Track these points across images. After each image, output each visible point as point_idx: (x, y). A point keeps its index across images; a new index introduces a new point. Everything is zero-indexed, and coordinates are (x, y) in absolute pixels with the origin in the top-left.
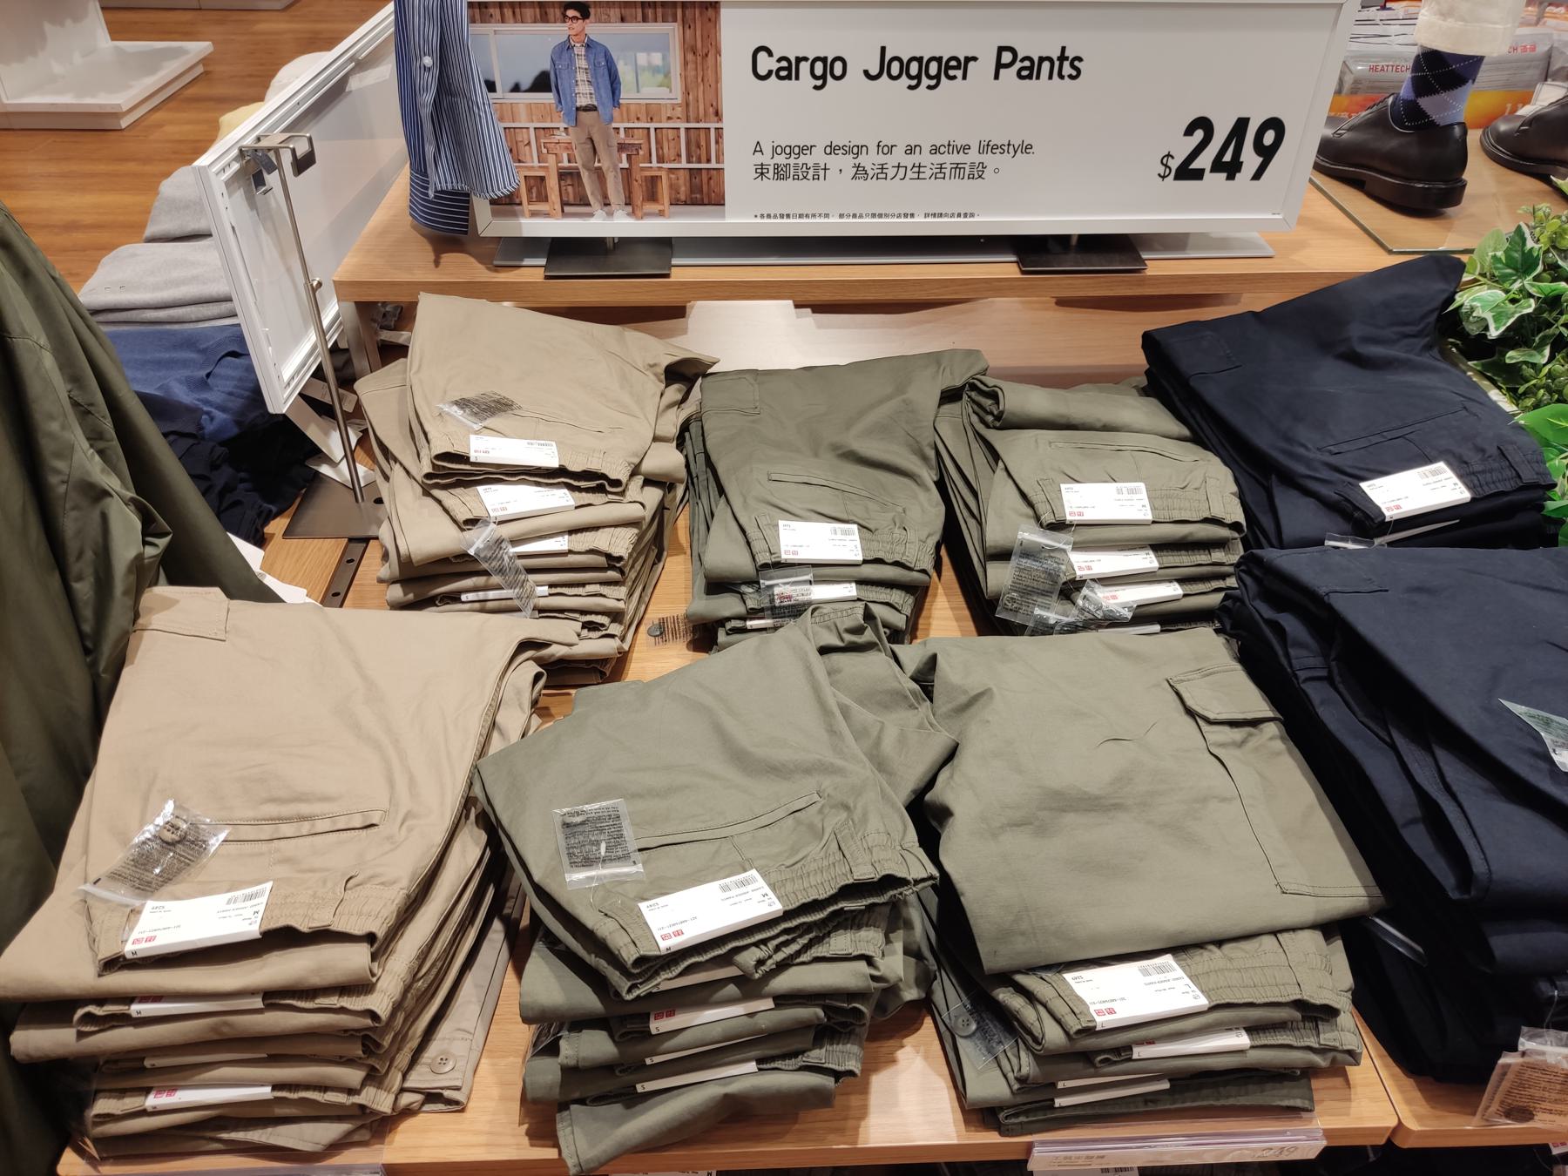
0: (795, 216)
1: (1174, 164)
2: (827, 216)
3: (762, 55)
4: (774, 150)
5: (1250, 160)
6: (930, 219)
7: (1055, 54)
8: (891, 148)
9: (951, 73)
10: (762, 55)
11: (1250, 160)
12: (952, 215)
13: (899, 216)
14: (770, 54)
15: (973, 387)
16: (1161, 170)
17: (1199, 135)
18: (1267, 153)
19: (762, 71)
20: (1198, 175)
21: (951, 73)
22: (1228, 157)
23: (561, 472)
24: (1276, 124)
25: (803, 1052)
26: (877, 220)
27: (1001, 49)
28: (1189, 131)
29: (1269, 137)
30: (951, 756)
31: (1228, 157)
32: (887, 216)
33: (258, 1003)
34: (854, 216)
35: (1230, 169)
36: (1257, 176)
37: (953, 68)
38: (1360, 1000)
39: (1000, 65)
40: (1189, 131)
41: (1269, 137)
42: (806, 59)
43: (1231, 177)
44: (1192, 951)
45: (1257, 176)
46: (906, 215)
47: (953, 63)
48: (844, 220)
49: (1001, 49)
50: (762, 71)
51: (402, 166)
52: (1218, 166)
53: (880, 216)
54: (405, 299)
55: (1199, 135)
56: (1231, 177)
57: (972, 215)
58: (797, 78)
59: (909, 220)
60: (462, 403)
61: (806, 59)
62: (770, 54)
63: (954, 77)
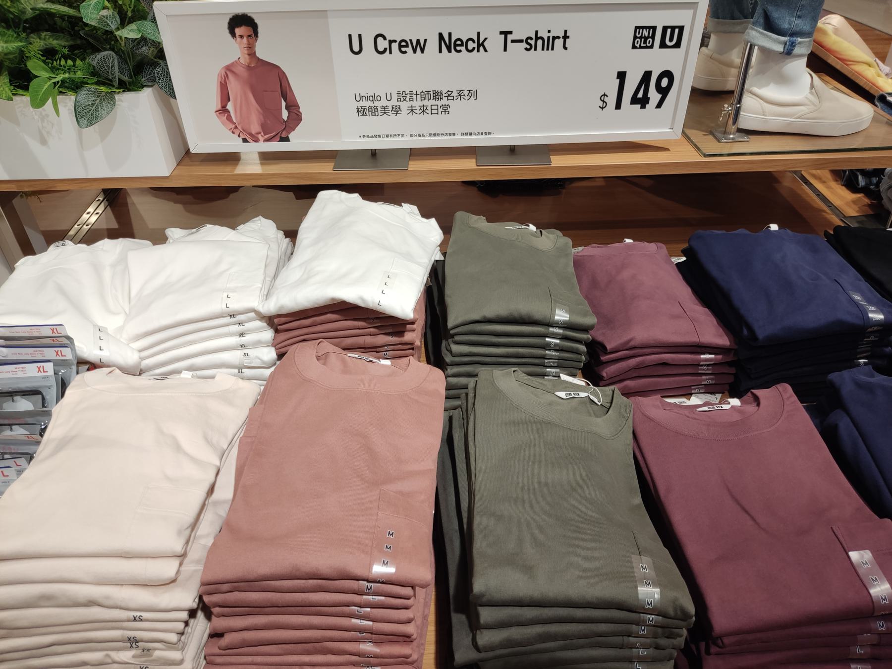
0: (383, 136)
2: (403, 135)
3: (380, 39)
5: (654, 96)
6: (465, 137)
7: (562, 34)
9: (458, 48)
10: (380, 39)
11: (654, 96)
12: (478, 134)
13: (446, 135)
14: (385, 38)
15: (223, 110)
16: (601, 103)
18: (664, 92)
19: (381, 49)
21: (458, 48)
22: (640, 95)
26: (433, 138)
29: (665, 82)
31: (640, 95)
32: (439, 135)
34: (419, 135)
35: (641, 101)
36: (659, 105)
37: (404, 46)
38: (696, 615)
41: (665, 82)
42: (395, 41)
43: (643, 107)
45: (659, 105)
46: (450, 135)
47: (459, 42)
48: (414, 138)
50: (381, 49)
51: (63, 444)
52: (634, 100)
53: (435, 135)
54: (135, 231)
56: (643, 107)
57: (490, 133)
58: (553, 49)
59: (452, 137)
61: (395, 41)
62: (385, 38)
63: (460, 51)
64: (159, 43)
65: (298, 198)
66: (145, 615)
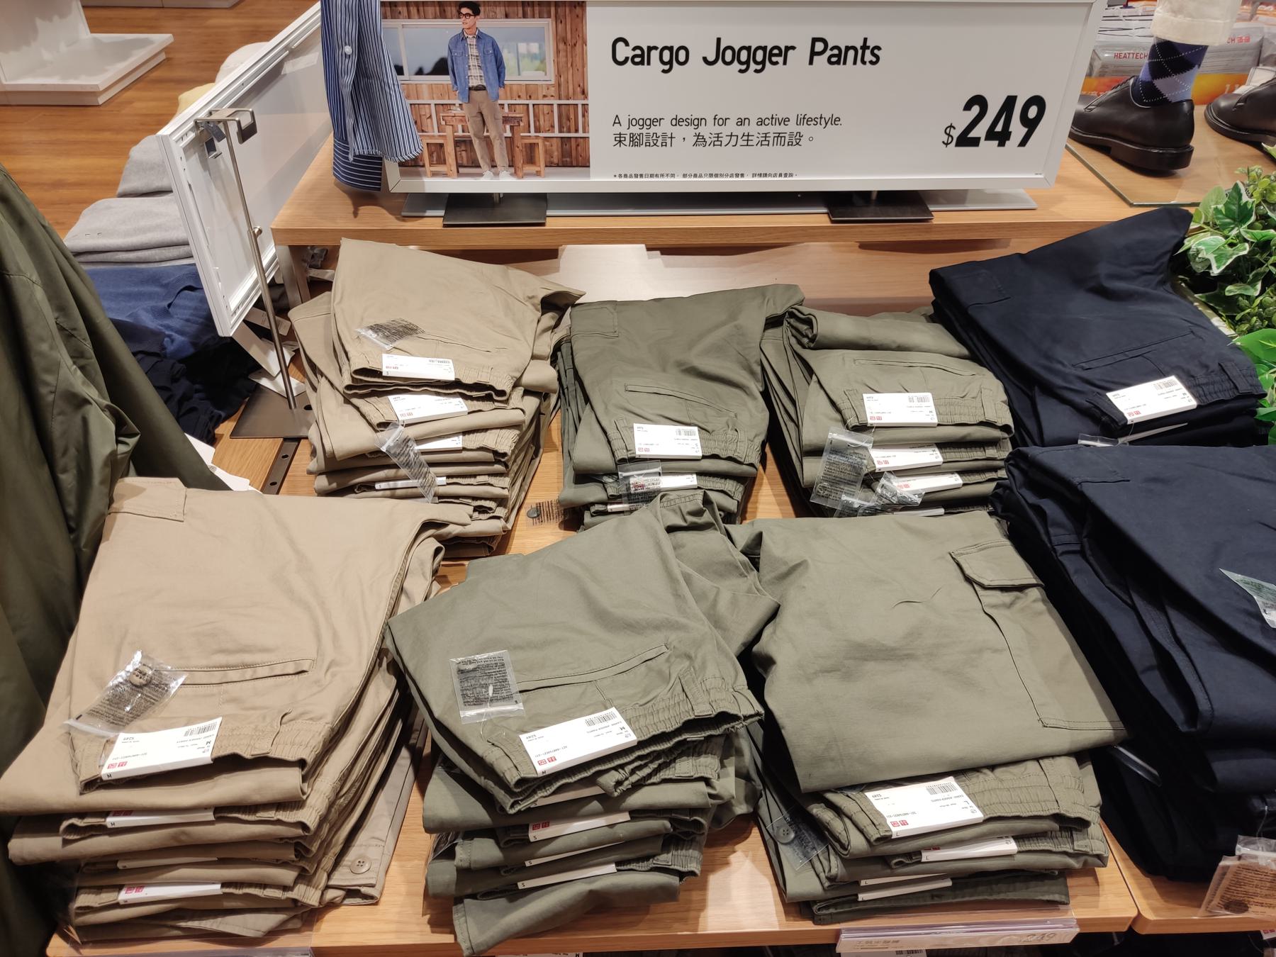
0: (647, 176)
1: (956, 134)
2: (673, 175)
3: (620, 45)
4: (630, 122)
5: (1018, 130)
6: (757, 179)
7: (859, 44)
8: (725, 121)
9: (774, 59)
10: (620, 45)
11: (1018, 130)
12: (775, 175)
13: (732, 176)
14: (627, 44)
16: (945, 138)
17: (976, 110)
18: (1031, 125)
19: (620, 58)
20: (975, 142)
21: (774, 59)
22: (999, 128)
23: (457, 384)
24: (1038, 101)
25: (653, 856)
26: (713, 179)
27: (814, 40)
28: (968, 107)
29: (1033, 112)
30: (774, 615)
31: (999, 128)
32: (722, 175)
33: (210, 816)
34: (695, 176)
35: (1001, 137)
36: (1023, 143)
37: (776, 55)
38: (1107, 813)
39: (813, 53)
40: (968, 107)
41: (1033, 112)
42: (656, 48)
43: (1002, 144)
44: (970, 774)
45: (1023, 143)
46: (737, 175)
47: (776, 51)
48: (687, 179)
49: (814, 40)
50: (620, 58)
52: (991, 135)
53: (716, 176)
54: (329, 243)
55: (976, 110)
56: (1002, 144)
57: (791, 175)
58: (649, 63)
59: (740, 179)
60: (376, 328)
61: (656, 48)
62: (627, 44)
63: (777, 63)
64: (128, 727)
65: (662, 254)
66: (111, 821)
